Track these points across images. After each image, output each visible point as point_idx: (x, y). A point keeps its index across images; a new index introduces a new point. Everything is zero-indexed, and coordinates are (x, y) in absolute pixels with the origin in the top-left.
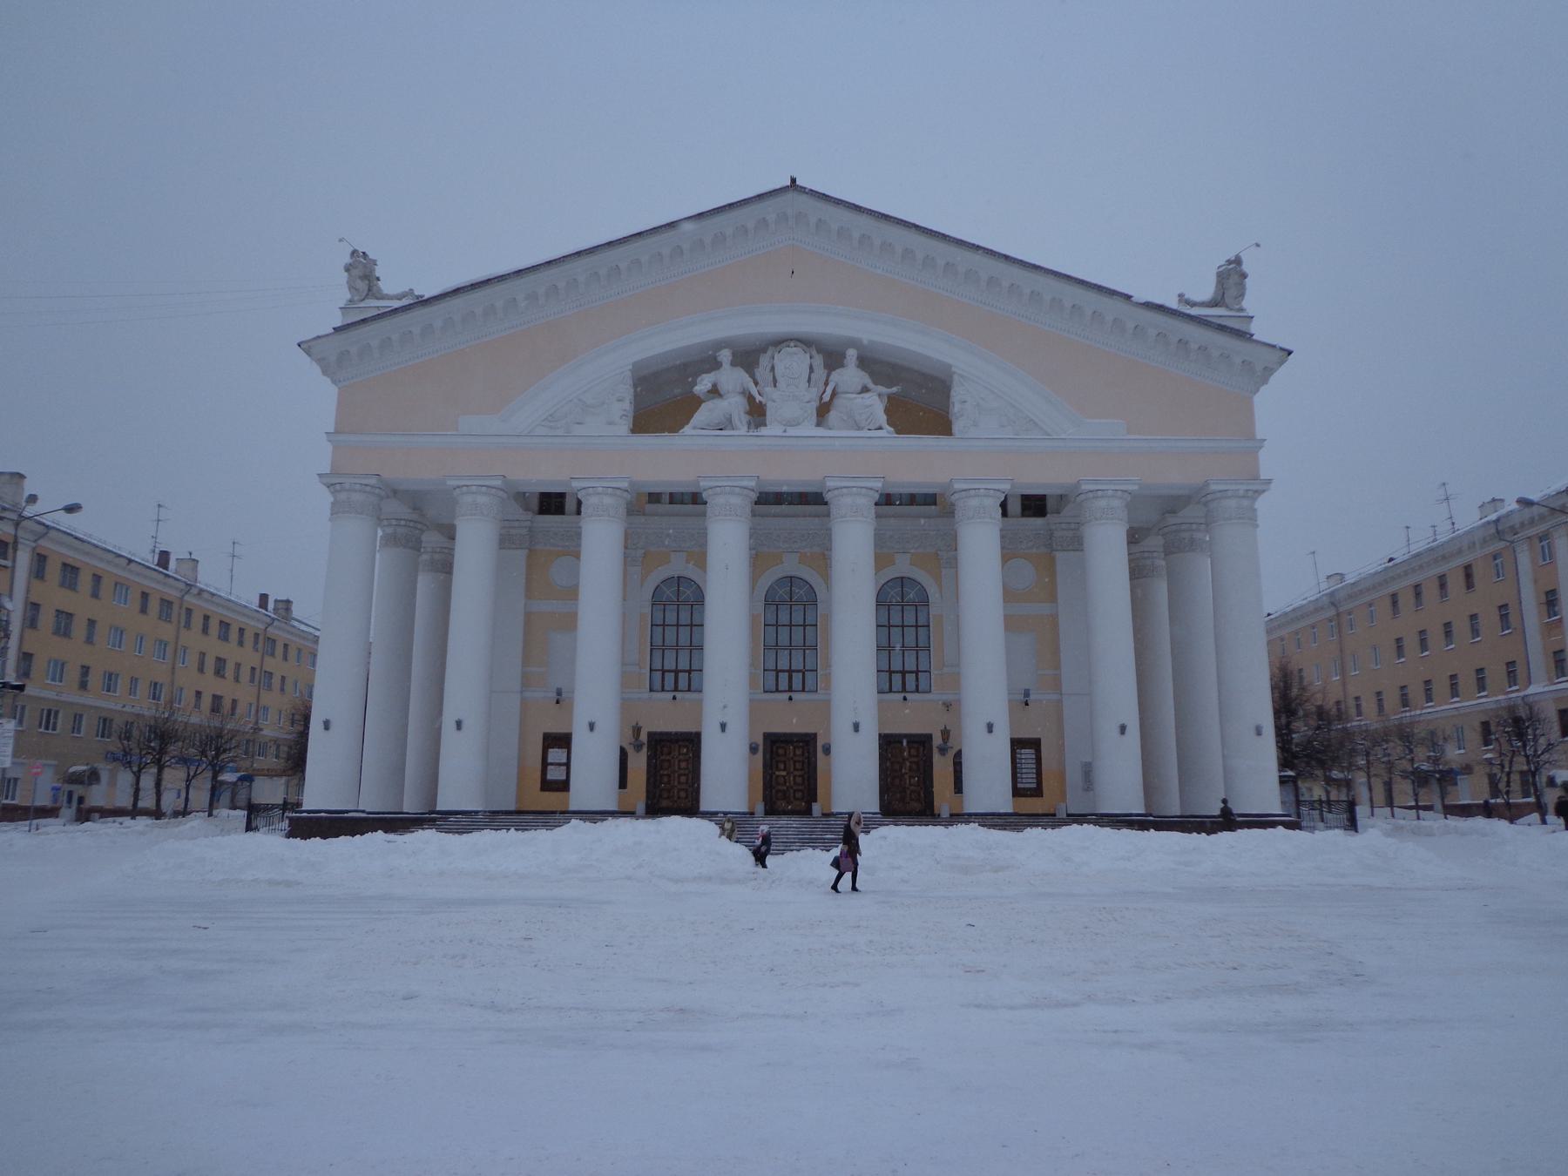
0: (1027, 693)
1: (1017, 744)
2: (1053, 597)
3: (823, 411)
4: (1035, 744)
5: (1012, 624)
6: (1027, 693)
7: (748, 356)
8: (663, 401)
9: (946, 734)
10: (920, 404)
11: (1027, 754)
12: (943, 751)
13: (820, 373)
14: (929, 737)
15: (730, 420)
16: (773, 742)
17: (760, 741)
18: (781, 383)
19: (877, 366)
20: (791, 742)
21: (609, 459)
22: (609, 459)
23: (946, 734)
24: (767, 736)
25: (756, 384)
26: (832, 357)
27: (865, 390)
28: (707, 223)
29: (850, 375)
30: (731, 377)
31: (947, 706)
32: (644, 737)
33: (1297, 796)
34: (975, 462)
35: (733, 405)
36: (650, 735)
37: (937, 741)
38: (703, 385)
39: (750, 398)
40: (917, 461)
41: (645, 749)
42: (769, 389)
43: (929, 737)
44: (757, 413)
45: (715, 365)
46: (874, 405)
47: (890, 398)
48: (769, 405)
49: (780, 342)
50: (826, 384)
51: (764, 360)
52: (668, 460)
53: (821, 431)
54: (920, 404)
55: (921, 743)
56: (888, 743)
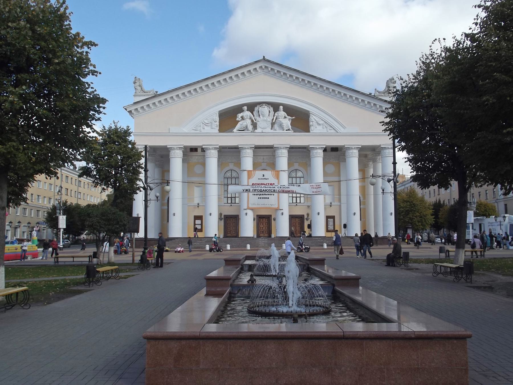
0: (331, 204)
1: (328, 217)
2: (339, 176)
3: (273, 124)
4: (333, 217)
5: (359, 170)
6: (331, 204)
7: (251, 107)
8: (228, 119)
9: (308, 215)
10: (301, 120)
11: (331, 221)
12: (307, 219)
13: (272, 113)
14: (304, 215)
15: (247, 127)
16: (259, 217)
17: (256, 217)
18: (261, 116)
19: (289, 110)
20: (264, 217)
21: (214, 139)
22: (214, 139)
23: (308, 215)
24: (257, 216)
25: (254, 116)
26: (276, 107)
27: (285, 117)
28: (153, 342)
29: (282, 113)
30: (247, 114)
31: (309, 207)
32: (223, 217)
33: (109, 255)
34: (316, 138)
35: (248, 122)
36: (224, 215)
37: (306, 217)
38: (240, 115)
39: (252, 121)
40: (300, 139)
41: (223, 221)
42: (258, 118)
43: (304, 215)
44: (255, 126)
45: (242, 111)
46: (287, 122)
47: (292, 119)
48: (258, 123)
49: (260, 104)
50: (274, 116)
51: (256, 109)
52: (229, 140)
53: (272, 131)
54: (301, 120)
55: (301, 218)
56: (292, 217)
